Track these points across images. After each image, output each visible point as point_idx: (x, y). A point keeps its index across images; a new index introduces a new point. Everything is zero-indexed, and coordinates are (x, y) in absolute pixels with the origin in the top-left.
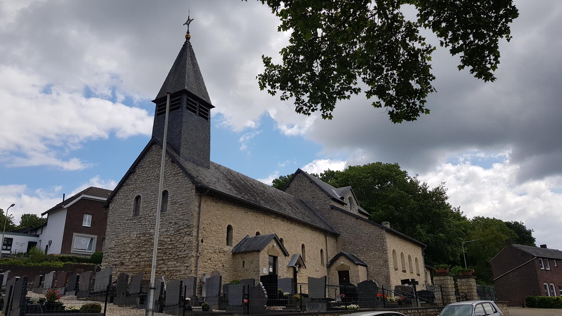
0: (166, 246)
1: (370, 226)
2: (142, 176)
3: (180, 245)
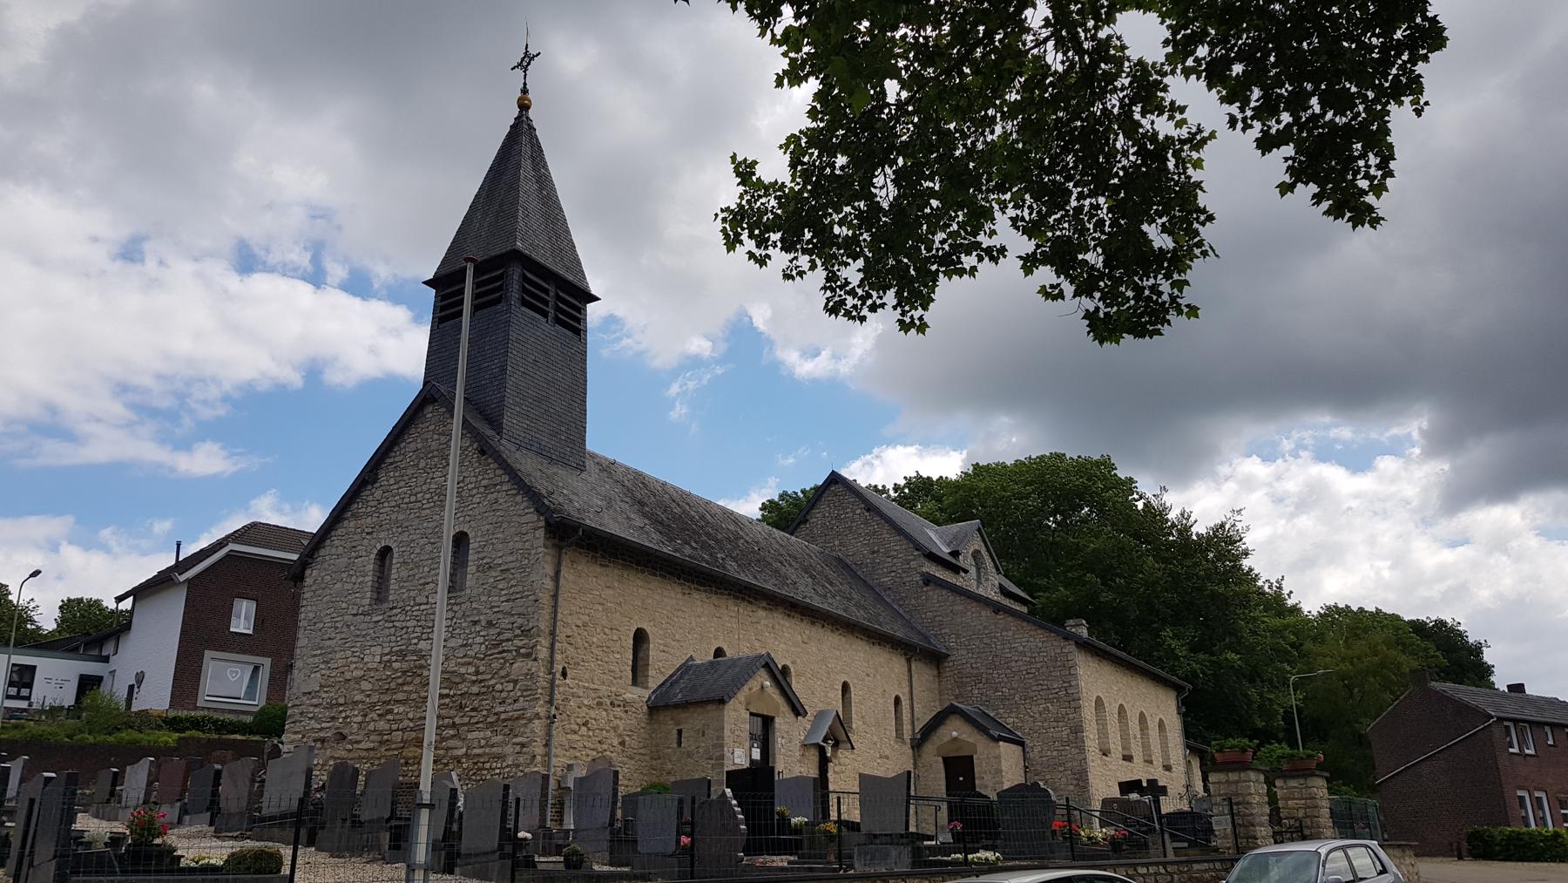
0: (463, 688)
1: (1032, 633)
2: (396, 491)
3: (502, 684)
